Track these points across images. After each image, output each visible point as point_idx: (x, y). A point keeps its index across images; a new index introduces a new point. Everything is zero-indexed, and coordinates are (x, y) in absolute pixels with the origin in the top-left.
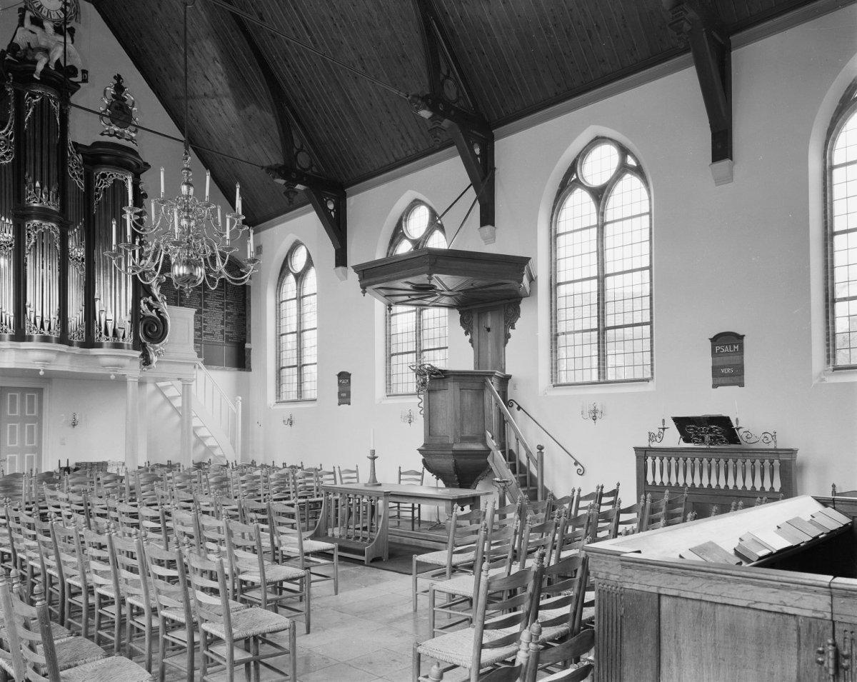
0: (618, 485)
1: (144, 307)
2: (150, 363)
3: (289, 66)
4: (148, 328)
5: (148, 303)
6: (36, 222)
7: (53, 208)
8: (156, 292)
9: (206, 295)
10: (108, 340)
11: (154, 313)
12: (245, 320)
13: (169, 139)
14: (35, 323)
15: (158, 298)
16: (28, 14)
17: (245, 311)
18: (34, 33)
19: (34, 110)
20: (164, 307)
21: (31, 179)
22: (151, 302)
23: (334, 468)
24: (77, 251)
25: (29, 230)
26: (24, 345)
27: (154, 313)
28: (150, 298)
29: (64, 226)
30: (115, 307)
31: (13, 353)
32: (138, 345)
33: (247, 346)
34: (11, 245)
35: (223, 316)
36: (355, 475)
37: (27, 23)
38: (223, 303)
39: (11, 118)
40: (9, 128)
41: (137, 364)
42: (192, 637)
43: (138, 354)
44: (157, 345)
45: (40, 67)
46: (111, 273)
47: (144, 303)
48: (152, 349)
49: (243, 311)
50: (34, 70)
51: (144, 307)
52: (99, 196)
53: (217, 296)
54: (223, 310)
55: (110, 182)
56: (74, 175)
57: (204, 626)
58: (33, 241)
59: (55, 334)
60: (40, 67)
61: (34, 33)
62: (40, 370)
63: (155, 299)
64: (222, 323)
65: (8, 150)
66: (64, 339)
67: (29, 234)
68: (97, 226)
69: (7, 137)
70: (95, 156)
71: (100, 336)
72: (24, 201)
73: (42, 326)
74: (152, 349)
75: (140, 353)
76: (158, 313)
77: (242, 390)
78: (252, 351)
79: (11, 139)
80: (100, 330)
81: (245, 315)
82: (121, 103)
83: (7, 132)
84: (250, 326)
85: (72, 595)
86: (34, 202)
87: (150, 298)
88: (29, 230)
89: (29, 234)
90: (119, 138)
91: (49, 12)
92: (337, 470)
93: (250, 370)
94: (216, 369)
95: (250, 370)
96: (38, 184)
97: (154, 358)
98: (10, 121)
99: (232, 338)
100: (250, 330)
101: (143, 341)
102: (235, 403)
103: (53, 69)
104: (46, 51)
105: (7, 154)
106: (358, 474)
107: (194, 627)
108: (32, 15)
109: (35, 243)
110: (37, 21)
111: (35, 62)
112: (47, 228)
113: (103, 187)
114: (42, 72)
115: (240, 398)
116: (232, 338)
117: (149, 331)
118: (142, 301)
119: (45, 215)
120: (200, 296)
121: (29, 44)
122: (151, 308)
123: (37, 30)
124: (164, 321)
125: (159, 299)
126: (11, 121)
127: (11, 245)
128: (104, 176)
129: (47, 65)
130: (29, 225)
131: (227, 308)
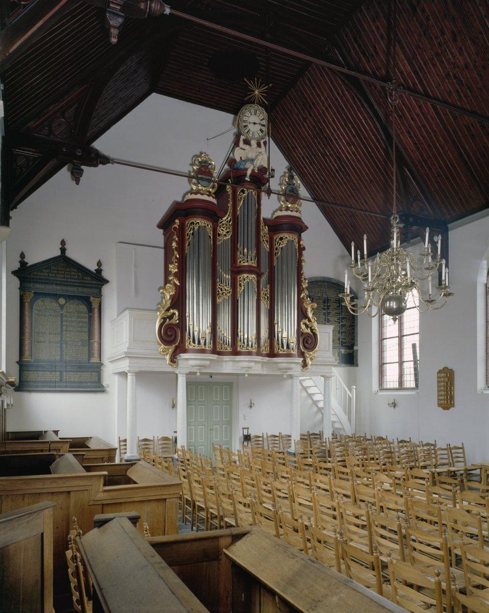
0: (435, 441)
1: (303, 327)
2: (307, 366)
3: (411, 137)
4: (305, 342)
5: (305, 324)
6: (245, 275)
7: (254, 265)
8: (310, 315)
9: (329, 313)
10: (284, 351)
11: (309, 331)
12: (354, 329)
13: (146, 247)
14: (244, 343)
15: (311, 319)
16: (242, 138)
17: (354, 323)
18: (244, 150)
19: (244, 201)
20: (315, 325)
21: (242, 247)
22: (308, 323)
23: (372, 436)
24: (265, 291)
25: (240, 281)
26: (238, 358)
27: (309, 331)
28: (307, 319)
29: (259, 275)
30: (287, 329)
31: (231, 363)
32: (302, 354)
33: (355, 348)
34: (229, 292)
35: (339, 327)
36: (461, 451)
37: (241, 144)
38: (340, 318)
39: (230, 208)
40: (229, 215)
41: (299, 367)
42: (220, 523)
43: (301, 360)
44: (311, 353)
45: (249, 172)
46: (285, 306)
47: (303, 324)
48: (308, 356)
49: (353, 323)
50: (245, 175)
51: (303, 327)
52: (278, 253)
53: (336, 313)
54: (339, 323)
55: (285, 242)
56: (263, 240)
57: (226, 519)
58: (243, 288)
59: (209, 347)
60: (249, 172)
61: (244, 150)
62: (245, 374)
63: (310, 321)
64: (339, 333)
65: (228, 230)
66: (259, 354)
67: (240, 284)
68: (276, 273)
69: (227, 222)
70: (276, 226)
71: (279, 349)
72: (237, 262)
73: (248, 345)
74: (308, 356)
75: (302, 359)
76: (312, 330)
77: (351, 381)
78: (358, 352)
79: (230, 222)
80: (278, 344)
81: (354, 326)
82: (293, 187)
83: (227, 218)
84: (357, 333)
85: (212, 519)
86: (244, 262)
87: (307, 319)
88: (240, 281)
89: (240, 284)
90: (292, 211)
91: (253, 134)
92: (373, 437)
93: (357, 365)
94: (454, 388)
95: (357, 365)
96: (246, 250)
97: (309, 362)
98: (229, 211)
99: (345, 343)
100: (357, 336)
101: (303, 350)
102: (350, 390)
103: (257, 172)
104: (252, 160)
105: (227, 232)
106: (464, 451)
107: (222, 518)
108: (244, 138)
109: (244, 290)
110: (247, 142)
111: (247, 169)
112: (251, 278)
113: (281, 246)
114: (251, 176)
115: (355, 387)
116: (345, 343)
117: (308, 341)
118: (302, 323)
119: (250, 270)
120: (324, 314)
121: (241, 158)
122: (307, 326)
123: (247, 147)
124: (315, 335)
125: (313, 320)
126: (230, 210)
127: (229, 292)
128: (281, 239)
129: (253, 170)
130: (240, 278)
131: (342, 322)
